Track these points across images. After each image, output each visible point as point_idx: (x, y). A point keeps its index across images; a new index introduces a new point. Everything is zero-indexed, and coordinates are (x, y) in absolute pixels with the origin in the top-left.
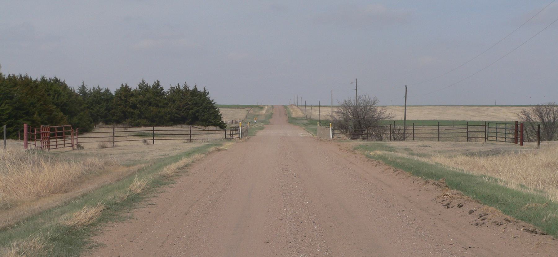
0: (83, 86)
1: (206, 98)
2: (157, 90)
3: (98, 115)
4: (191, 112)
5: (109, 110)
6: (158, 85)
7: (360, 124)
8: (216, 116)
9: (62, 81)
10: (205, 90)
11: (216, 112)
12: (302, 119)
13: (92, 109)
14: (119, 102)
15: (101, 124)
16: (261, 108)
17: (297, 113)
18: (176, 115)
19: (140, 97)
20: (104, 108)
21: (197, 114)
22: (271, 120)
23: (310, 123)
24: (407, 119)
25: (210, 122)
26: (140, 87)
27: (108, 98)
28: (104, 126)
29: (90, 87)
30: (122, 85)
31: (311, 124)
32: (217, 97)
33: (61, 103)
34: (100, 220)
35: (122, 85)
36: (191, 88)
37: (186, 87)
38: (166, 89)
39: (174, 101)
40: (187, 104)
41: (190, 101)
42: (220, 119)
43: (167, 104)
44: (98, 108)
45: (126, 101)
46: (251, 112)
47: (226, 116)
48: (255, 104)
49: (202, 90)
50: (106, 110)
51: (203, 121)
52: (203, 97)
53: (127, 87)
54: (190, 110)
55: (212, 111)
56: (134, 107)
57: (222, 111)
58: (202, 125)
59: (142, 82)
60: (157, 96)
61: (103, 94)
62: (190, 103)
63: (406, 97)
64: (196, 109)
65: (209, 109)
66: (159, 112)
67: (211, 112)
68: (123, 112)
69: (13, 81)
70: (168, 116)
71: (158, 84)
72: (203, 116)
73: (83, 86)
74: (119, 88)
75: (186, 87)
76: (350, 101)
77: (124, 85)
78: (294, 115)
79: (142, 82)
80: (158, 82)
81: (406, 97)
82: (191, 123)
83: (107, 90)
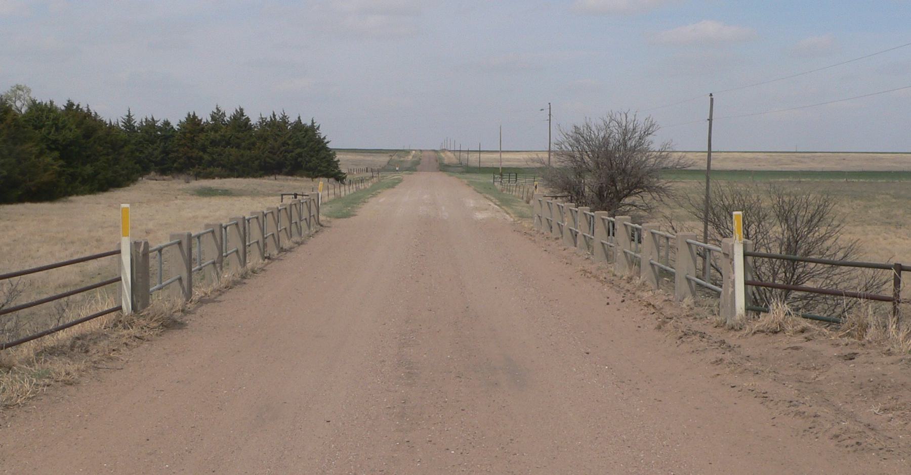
0: (129, 116)
1: (315, 135)
2: (240, 122)
3: (151, 161)
4: (289, 155)
5: (167, 153)
6: (242, 115)
7: (607, 179)
8: (328, 161)
9: (83, 106)
10: (313, 123)
11: (330, 155)
12: (456, 166)
13: (141, 152)
14: (183, 141)
15: (153, 173)
16: (408, 152)
17: (449, 158)
18: (268, 160)
19: (212, 135)
20: (160, 150)
21: (299, 160)
22: (418, 167)
23: (494, 176)
24: (712, 167)
25: (320, 171)
26: (213, 118)
27: (169, 134)
28: (157, 177)
29: (138, 119)
30: (189, 115)
31: (468, 172)
32: (335, 136)
33: (64, 140)
34: (413, 167)
35: (189, 115)
36: (292, 119)
37: (284, 118)
38: (254, 120)
39: (265, 140)
40: (285, 144)
41: (290, 138)
42: (337, 167)
43: (254, 144)
44: (150, 150)
45: (192, 140)
46: (395, 157)
47: (344, 162)
48: (402, 149)
49: (309, 124)
50: (163, 152)
51: (308, 169)
52: (310, 133)
53: (195, 117)
54: (289, 151)
55: (323, 154)
56: (204, 149)
57: (338, 157)
58: (308, 176)
59: (215, 111)
60: (239, 131)
61: (160, 129)
62: (290, 142)
63: (710, 120)
64: (299, 150)
65: (318, 151)
66: (242, 156)
67: (323, 156)
68: (189, 158)
69: (41, 114)
70: (257, 163)
71: (241, 112)
72: (310, 161)
73: (129, 116)
74: (183, 120)
75: (284, 118)
76: (589, 127)
77: (192, 114)
78: (446, 162)
79: (215, 111)
80: (241, 110)
81: (710, 120)
82: (291, 173)
83: (167, 123)
